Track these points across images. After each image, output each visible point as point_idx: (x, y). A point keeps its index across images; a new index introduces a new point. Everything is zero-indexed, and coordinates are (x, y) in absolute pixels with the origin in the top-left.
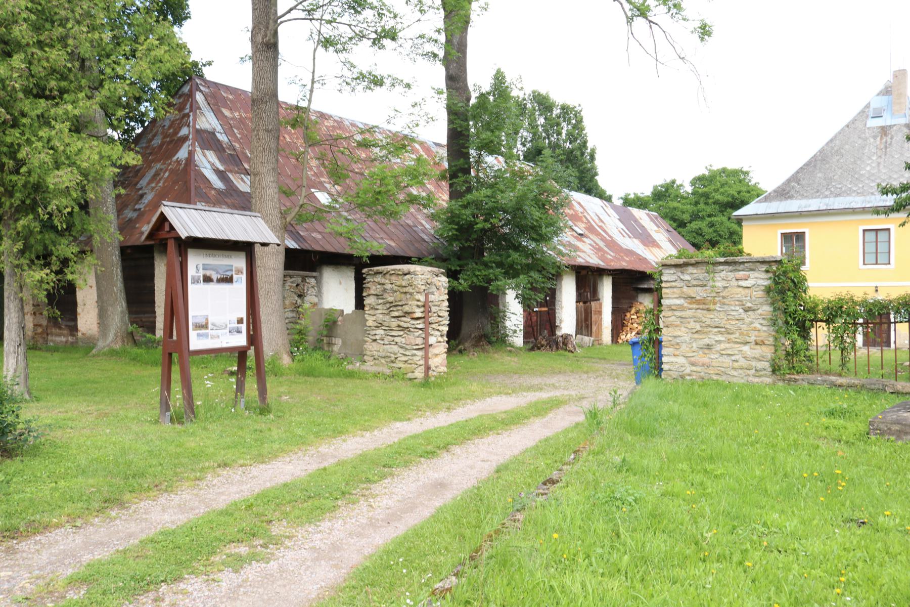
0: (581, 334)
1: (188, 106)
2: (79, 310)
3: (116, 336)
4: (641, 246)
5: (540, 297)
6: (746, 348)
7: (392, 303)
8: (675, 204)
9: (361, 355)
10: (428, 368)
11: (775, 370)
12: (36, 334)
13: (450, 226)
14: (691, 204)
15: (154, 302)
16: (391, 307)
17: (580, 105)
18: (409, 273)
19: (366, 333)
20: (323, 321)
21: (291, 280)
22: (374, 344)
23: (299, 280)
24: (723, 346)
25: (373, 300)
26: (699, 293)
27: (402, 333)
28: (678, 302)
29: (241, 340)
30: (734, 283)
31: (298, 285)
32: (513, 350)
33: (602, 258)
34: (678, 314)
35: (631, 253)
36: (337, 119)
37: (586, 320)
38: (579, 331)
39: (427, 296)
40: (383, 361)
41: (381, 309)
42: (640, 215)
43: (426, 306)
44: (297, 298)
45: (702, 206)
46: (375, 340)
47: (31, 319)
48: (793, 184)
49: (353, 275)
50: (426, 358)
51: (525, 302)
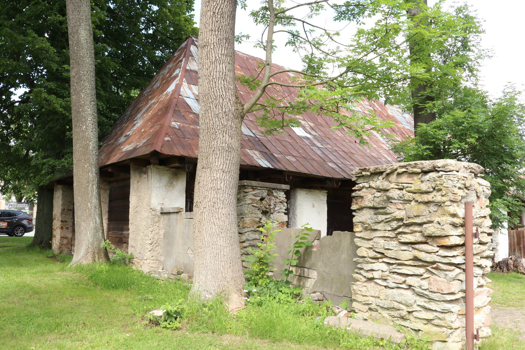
1: (183, 55)
3: (87, 253)
7: (402, 220)
12: (62, 244)
13: (425, 147)
15: (128, 220)
16: (399, 227)
19: (356, 266)
20: (292, 245)
21: (254, 192)
23: (265, 193)
25: (369, 216)
27: (421, 271)
31: (262, 199)
40: (385, 313)
44: (260, 215)
46: (371, 279)
47: (59, 233)
49: (325, 199)
50: (468, 315)
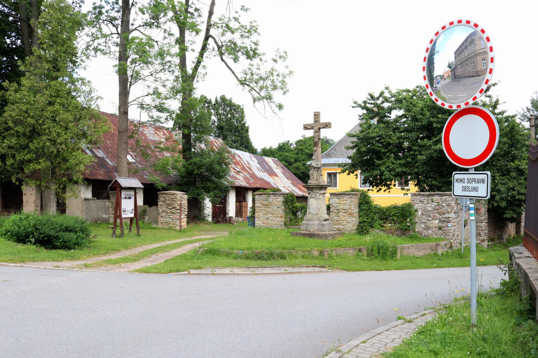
0: (238, 217)
2: (24, 204)
4: (268, 176)
5: (219, 200)
6: (278, 219)
8: (287, 154)
9: (157, 222)
10: (181, 226)
11: (285, 225)
14: (295, 154)
17: (243, 105)
18: (175, 194)
19: (159, 214)
22: (162, 218)
24: (272, 218)
26: (265, 203)
28: (259, 205)
29: (132, 215)
30: (275, 200)
32: (208, 223)
33: (247, 183)
34: (259, 208)
35: (262, 180)
36: (131, 120)
37: (240, 210)
38: (237, 215)
39: (181, 202)
41: (164, 206)
42: (269, 160)
43: (180, 205)
45: (300, 155)
48: (333, 151)
50: (180, 223)
51: (212, 202)
